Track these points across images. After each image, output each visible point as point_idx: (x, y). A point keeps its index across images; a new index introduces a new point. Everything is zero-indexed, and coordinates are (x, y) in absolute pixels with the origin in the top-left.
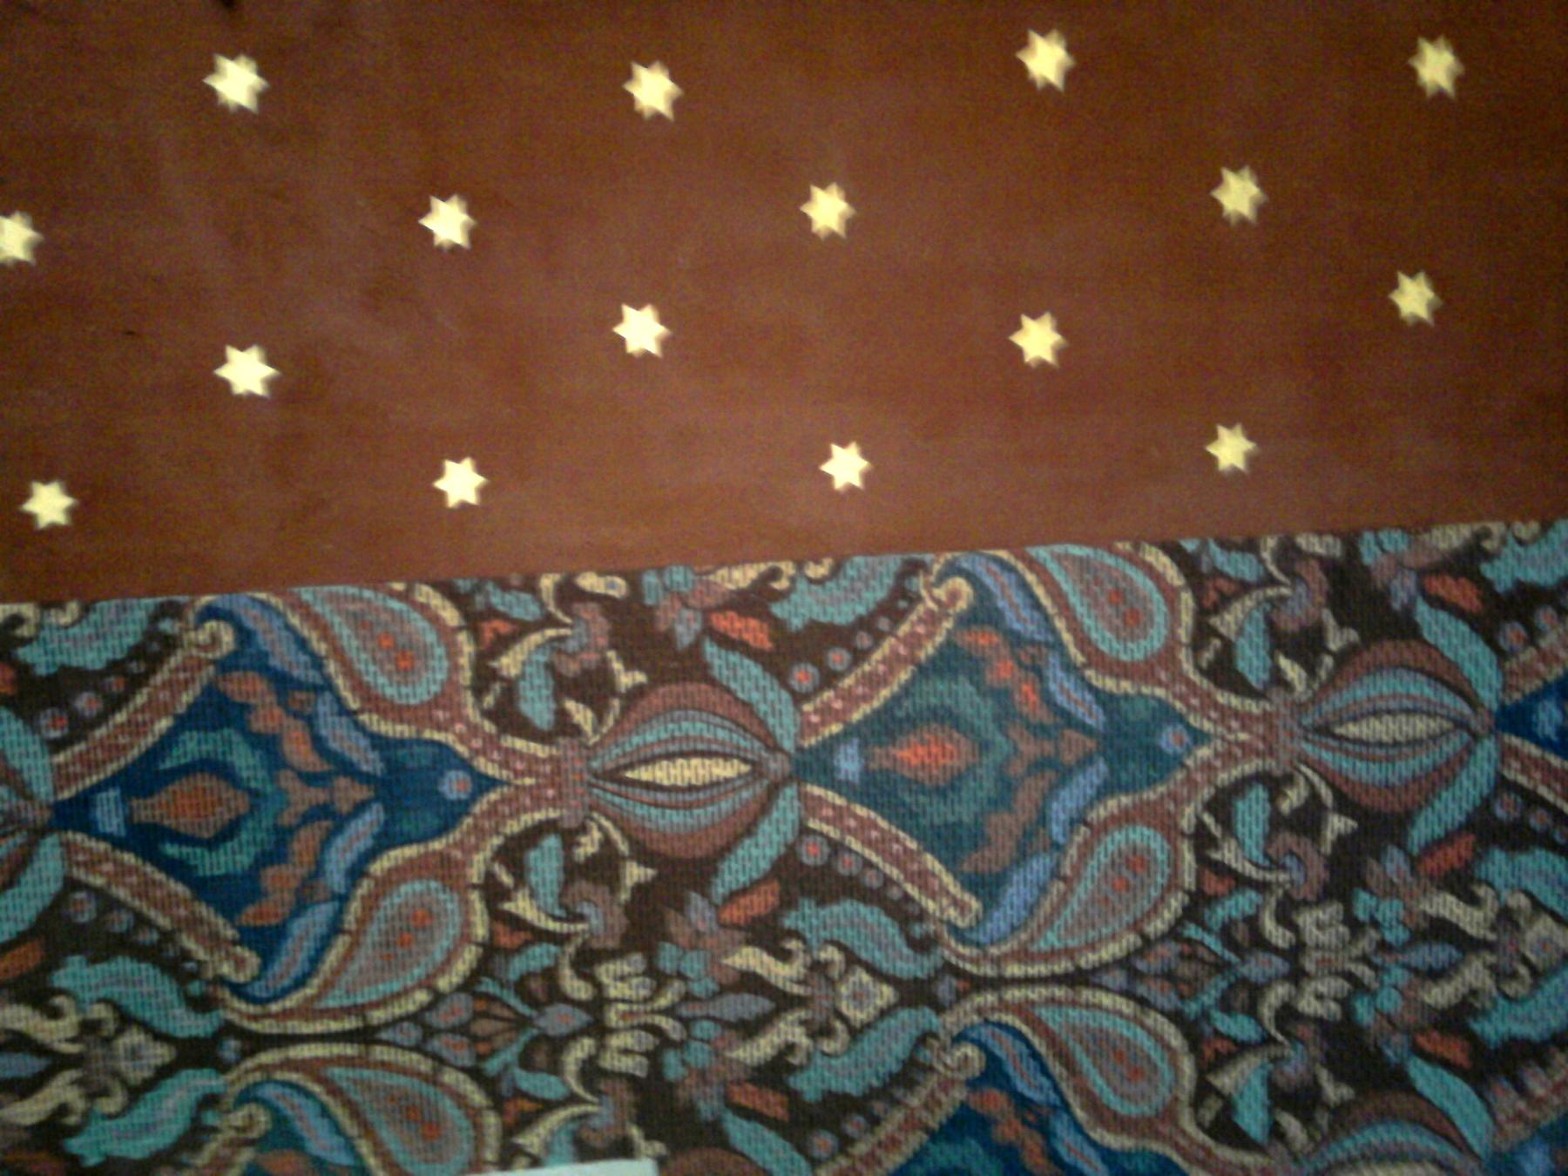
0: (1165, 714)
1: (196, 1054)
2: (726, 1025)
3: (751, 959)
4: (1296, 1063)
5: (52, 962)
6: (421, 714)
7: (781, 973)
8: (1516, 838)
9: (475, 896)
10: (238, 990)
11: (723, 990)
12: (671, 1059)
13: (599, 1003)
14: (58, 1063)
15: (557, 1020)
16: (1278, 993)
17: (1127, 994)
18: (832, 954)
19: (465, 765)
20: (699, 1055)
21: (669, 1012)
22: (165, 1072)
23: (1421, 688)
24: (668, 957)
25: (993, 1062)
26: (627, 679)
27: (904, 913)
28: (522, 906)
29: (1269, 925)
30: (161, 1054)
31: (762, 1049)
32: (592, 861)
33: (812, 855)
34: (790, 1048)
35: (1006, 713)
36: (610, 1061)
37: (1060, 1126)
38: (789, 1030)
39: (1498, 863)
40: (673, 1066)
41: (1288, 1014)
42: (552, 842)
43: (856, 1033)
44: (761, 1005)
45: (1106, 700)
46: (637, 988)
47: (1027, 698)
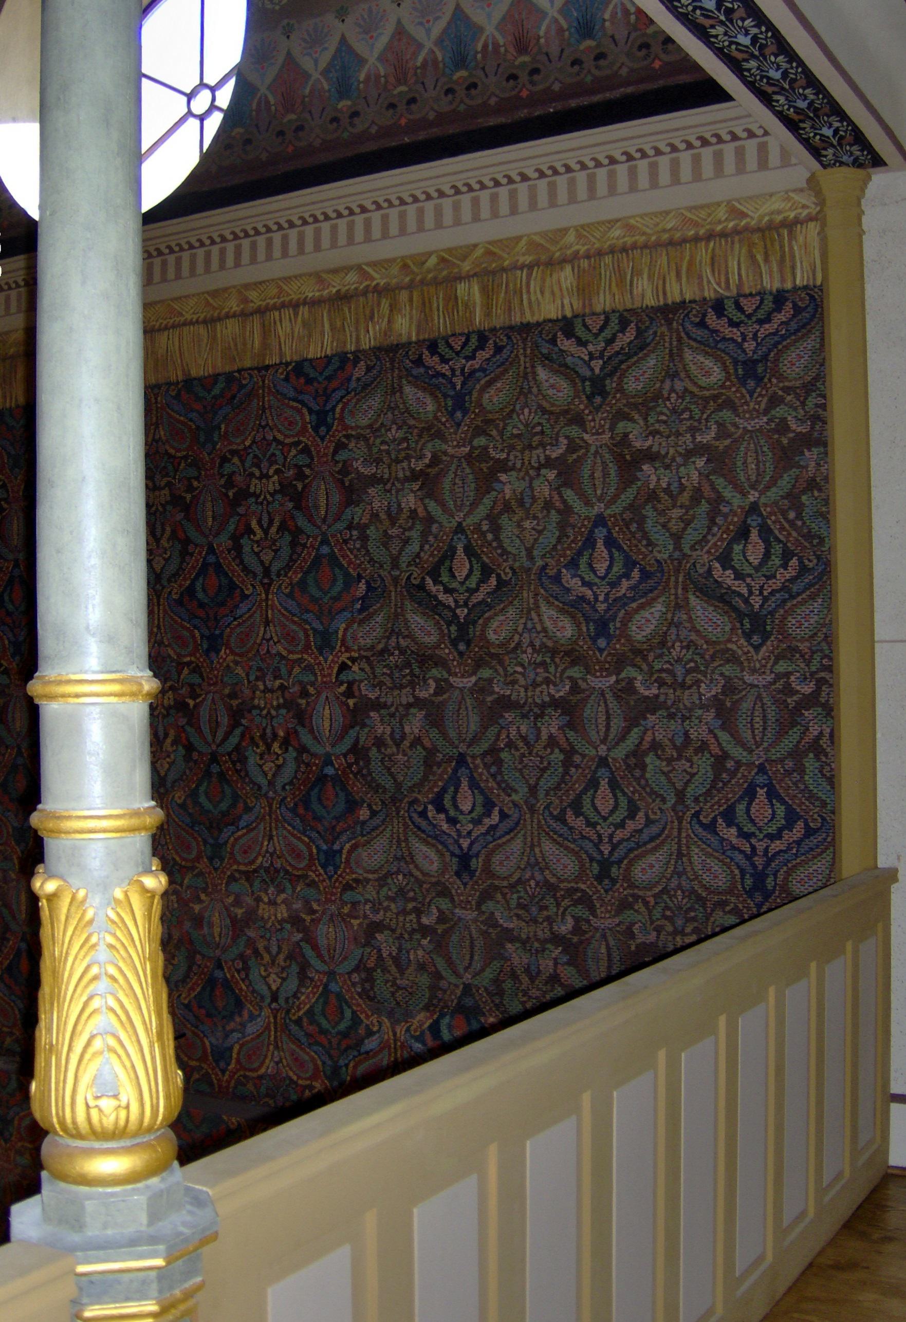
0: (329, 428)
1: (267, 571)
2: (264, 729)
3: (276, 524)
4: (238, 479)
5: (290, 532)
6: (342, 418)
7: (273, 530)
8: (293, 544)
9: (308, 1082)
10: (280, 586)
11: (269, 513)
12: (253, 500)
13: (267, 477)
14: (266, 532)
15: (265, 464)
16: (257, 473)
17: (267, 851)
18: (281, 761)
19: (327, 433)
20: (258, 720)
21: (265, 498)
22: (262, 562)
23: (334, 509)
24: (278, 497)
25: (247, 597)
26: (351, 702)
27: (288, 567)
28: (293, 452)
29: (283, 896)
30: (274, 988)
31: (254, 524)
32: (303, 472)
33: (191, 548)
34: (255, 535)
35: (329, 378)
36: (254, 481)
37: (232, 828)
38: (259, 534)
39: (288, 538)
40: (255, 712)
41: (252, 475)
42: (308, 461)
43: (261, 766)
44: (265, 525)
45: (333, 409)
46: (271, 488)
47: (334, 384)
